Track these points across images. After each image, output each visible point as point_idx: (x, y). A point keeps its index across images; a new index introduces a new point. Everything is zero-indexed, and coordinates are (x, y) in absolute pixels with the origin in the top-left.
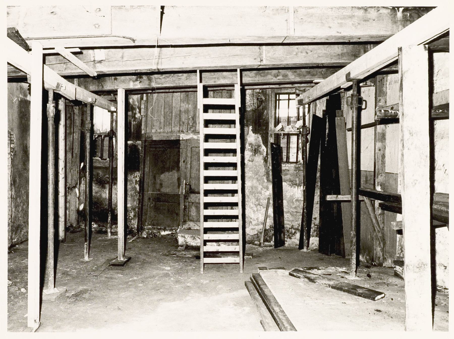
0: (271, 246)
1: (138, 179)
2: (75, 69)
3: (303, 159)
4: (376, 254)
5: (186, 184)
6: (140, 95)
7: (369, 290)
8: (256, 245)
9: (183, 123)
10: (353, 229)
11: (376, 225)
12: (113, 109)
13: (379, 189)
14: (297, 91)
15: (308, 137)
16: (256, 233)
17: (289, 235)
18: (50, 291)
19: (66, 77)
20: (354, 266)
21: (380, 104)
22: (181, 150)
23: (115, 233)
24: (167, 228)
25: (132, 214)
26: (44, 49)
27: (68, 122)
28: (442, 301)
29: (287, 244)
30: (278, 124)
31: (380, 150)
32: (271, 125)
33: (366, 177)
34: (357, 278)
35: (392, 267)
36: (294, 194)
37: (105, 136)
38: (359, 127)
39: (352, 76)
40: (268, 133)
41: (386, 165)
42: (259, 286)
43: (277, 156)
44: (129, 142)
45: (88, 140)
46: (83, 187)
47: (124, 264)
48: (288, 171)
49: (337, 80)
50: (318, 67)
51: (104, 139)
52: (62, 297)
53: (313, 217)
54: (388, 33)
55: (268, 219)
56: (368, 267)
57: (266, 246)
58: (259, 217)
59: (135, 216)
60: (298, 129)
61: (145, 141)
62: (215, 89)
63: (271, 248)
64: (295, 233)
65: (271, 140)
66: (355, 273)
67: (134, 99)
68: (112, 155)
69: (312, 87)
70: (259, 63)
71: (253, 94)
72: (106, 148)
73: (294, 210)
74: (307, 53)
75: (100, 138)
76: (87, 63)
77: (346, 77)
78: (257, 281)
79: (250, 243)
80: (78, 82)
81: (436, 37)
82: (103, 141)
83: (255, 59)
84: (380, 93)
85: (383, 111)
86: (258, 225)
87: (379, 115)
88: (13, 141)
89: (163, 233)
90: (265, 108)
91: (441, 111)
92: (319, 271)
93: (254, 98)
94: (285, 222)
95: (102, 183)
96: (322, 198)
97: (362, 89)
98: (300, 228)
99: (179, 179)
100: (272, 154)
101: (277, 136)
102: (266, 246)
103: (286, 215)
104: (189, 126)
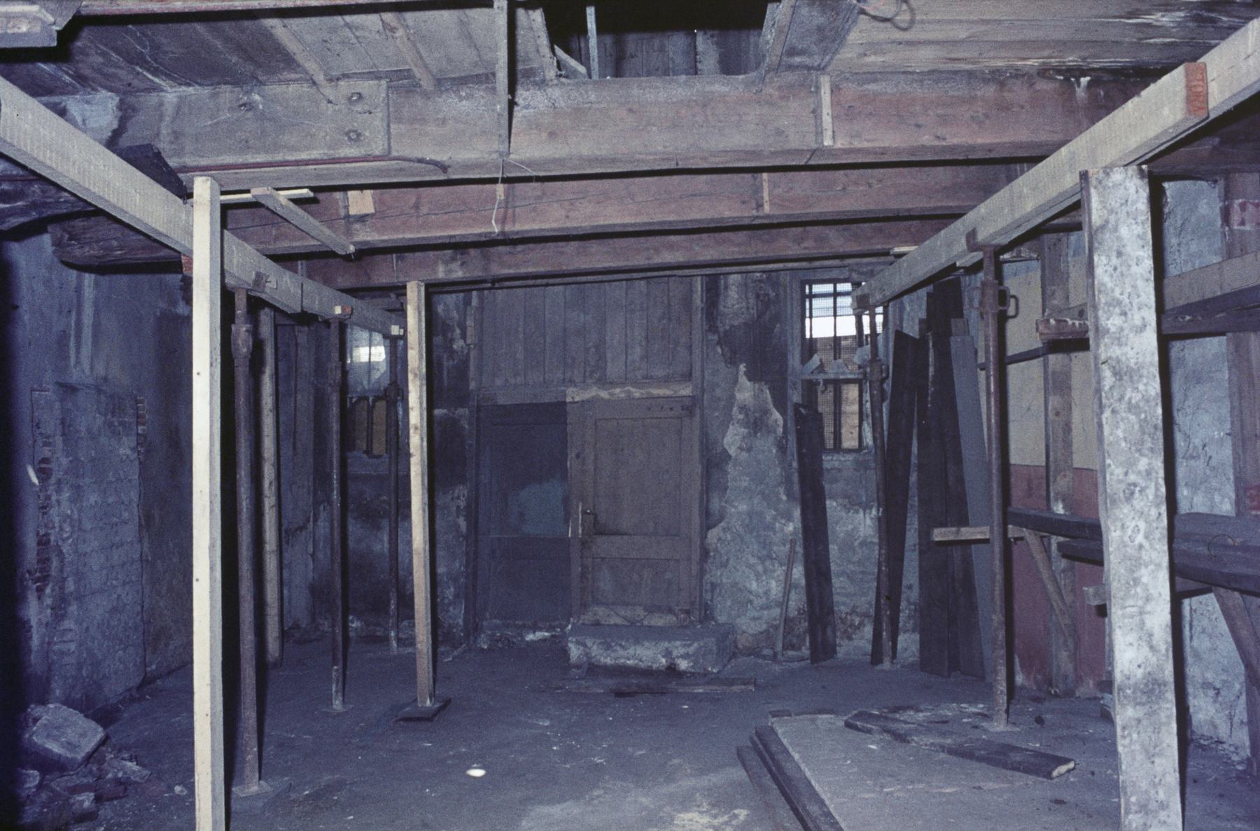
0: (803, 659)
1: (462, 504)
2: (301, 239)
3: (875, 439)
4: (1059, 667)
5: (584, 513)
6: (462, 295)
7: (1037, 754)
8: (764, 657)
9: (573, 359)
10: (998, 609)
11: (1054, 596)
12: (395, 330)
13: (1059, 509)
14: (855, 276)
15: (885, 386)
16: (764, 627)
17: (846, 631)
18: (252, 787)
19: (277, 258)
20: (1002, 699)
21: (1055, 302)
22: (569, 428)
23: (411, 641)
24: (540, 625)
25: (450, 592)
26: (223, 193)
27: (281, 365)
28: (1209, 772)
29: (841, 653)
30: (811, 356)
31: (1057, 414)
32: (794, 360)
33: (1029, 481)
34: (1009, 728)
35: (1095, 698)
36: (854, 526)
37: (377, 399)
38: (1003, 361)
39: (981, 237)
40: (786, 379)
41: (1074, 448)
42: (773, 759)
43: (809, 437)
44: (437, 412)
45: (335, 410)
46: (323, 527)
47: (435, 715)
48: (840, 470)
49: (948, 247)
50: (897, 218)
51: (373, 406)
52: (278, 802)
53: (905, 582)
54: (1057, 138)
55: (793, 592)
56: (1037, 700)
57: (790, 660)
58: (759, 585)
59: (457, 596)
60: (860, 367)
61: (479, 408)
62: (649, 274)
63: (802, 663)
64: (862, 624)
65: (796, 397)
66: (1005, 716)
67: (448, 304)
68: (400, 451)
69: (891, 264)
70: (754, 213)
71: (746, 284)
72: (380, 428)
73: (857, 569)
74: (870, 185)
75: (364, 405)
76: (330, 223)
77: (968, 241)
78: (765, 746)
79: (749, 655)
80: (308, 266)
81: (1162, 148)
82: (370, 410)
83: (744, 203)
84: (1053, 278)
85: (1052, 321)
86: (768, 607)
87: (1046, 331)
88: (142, 416)
89: (530, 637)
90: (777, 318)
91: (1188, 318)
92: (921, 715)
93: (750, 295)
94: (836, 598)
95: (371, 517)
96: (925, 534)
97: (1007, 268)
98: (872, 612)
99: (566, 501)
100: (798, 431)
101: (810, 388)
102: (790, 660)
103: (837, 582)
104: (588, 369)
